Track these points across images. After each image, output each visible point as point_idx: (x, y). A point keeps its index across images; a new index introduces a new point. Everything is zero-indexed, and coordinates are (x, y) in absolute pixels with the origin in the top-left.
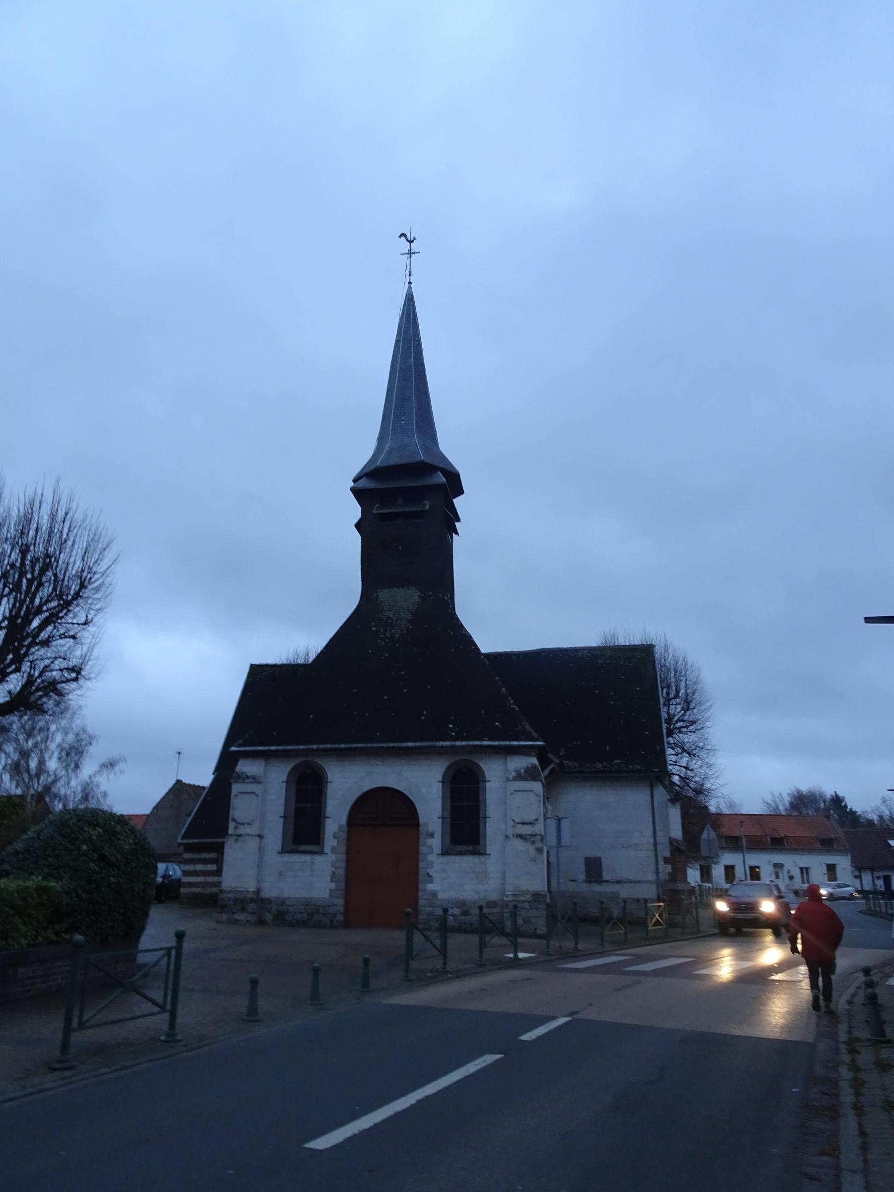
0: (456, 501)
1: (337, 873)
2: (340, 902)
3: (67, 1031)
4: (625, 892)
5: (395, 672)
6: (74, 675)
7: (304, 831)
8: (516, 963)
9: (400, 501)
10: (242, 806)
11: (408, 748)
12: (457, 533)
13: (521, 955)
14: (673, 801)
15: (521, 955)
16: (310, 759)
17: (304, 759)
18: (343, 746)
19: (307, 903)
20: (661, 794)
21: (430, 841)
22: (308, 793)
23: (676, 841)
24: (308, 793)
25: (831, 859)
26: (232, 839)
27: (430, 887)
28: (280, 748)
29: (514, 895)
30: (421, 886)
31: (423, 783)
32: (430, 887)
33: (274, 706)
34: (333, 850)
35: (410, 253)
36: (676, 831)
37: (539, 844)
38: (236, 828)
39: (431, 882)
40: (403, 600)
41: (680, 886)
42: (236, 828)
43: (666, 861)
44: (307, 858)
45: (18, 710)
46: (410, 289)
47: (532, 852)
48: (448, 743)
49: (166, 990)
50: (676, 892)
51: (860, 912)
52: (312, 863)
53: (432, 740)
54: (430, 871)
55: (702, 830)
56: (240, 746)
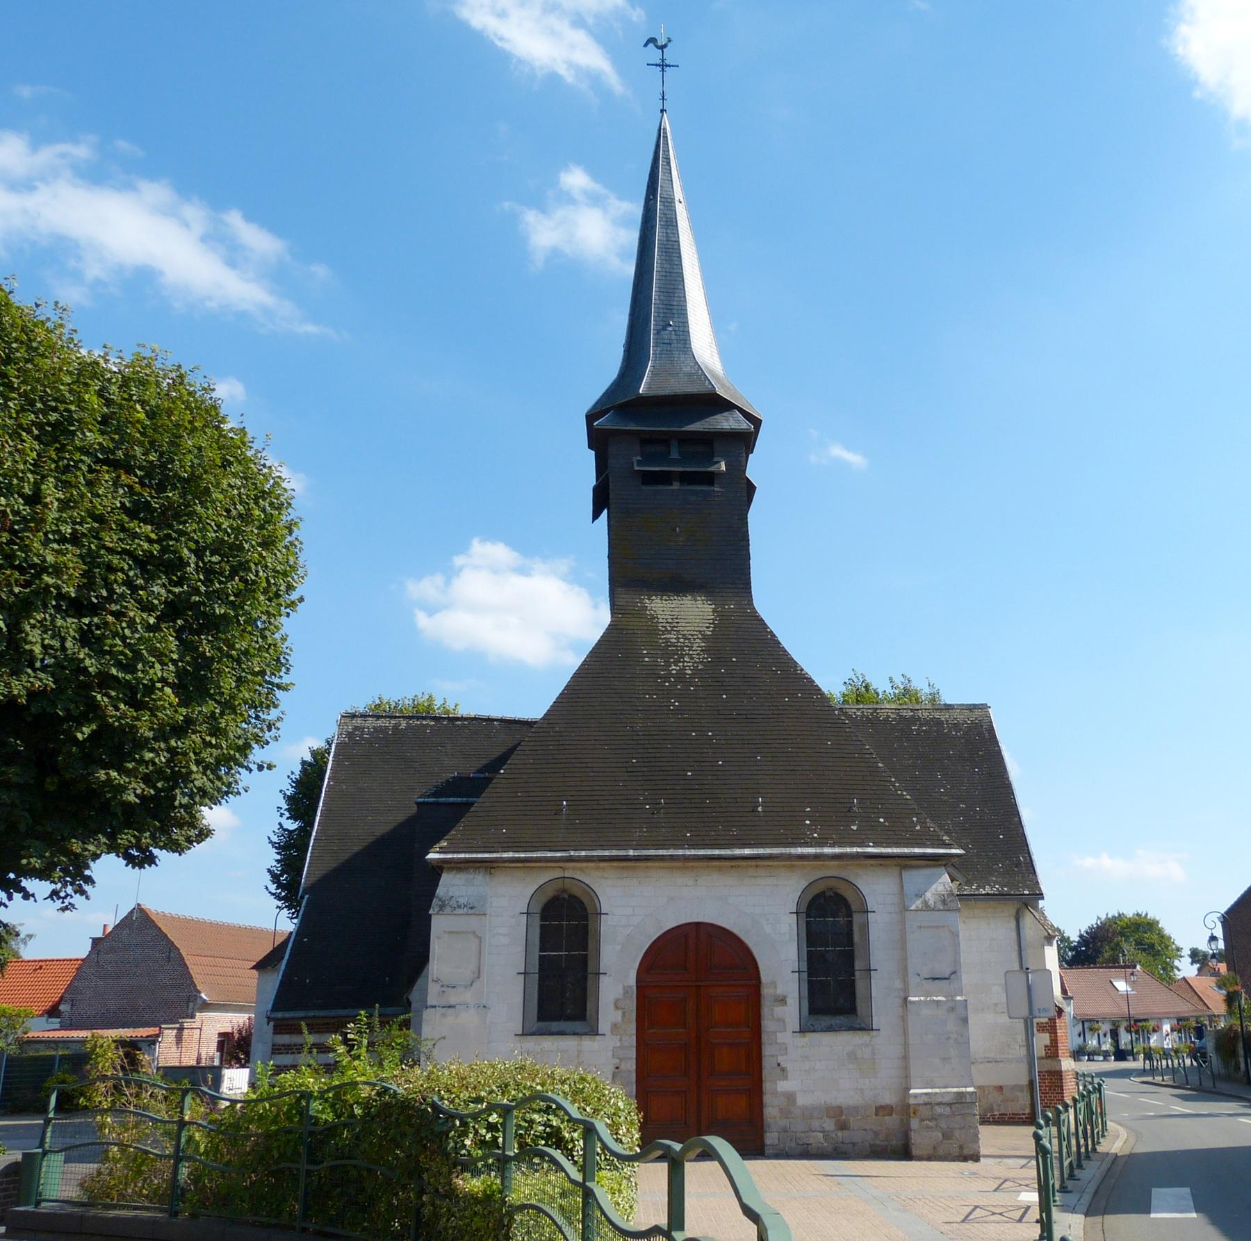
1: (623, 1067)
7: (560, 995)
9: (675, 455)
17: (558, 874)
21: (779, 1010)
22: (565, 929)
24: (565, 929)
27: (783, 1086)
30: (767, 1086)
32: (783, 1086)
34: (615, 1027)
39: (786, 1078)
40: (688, 614)
44: (568, 1043)
52: (579, 1052)
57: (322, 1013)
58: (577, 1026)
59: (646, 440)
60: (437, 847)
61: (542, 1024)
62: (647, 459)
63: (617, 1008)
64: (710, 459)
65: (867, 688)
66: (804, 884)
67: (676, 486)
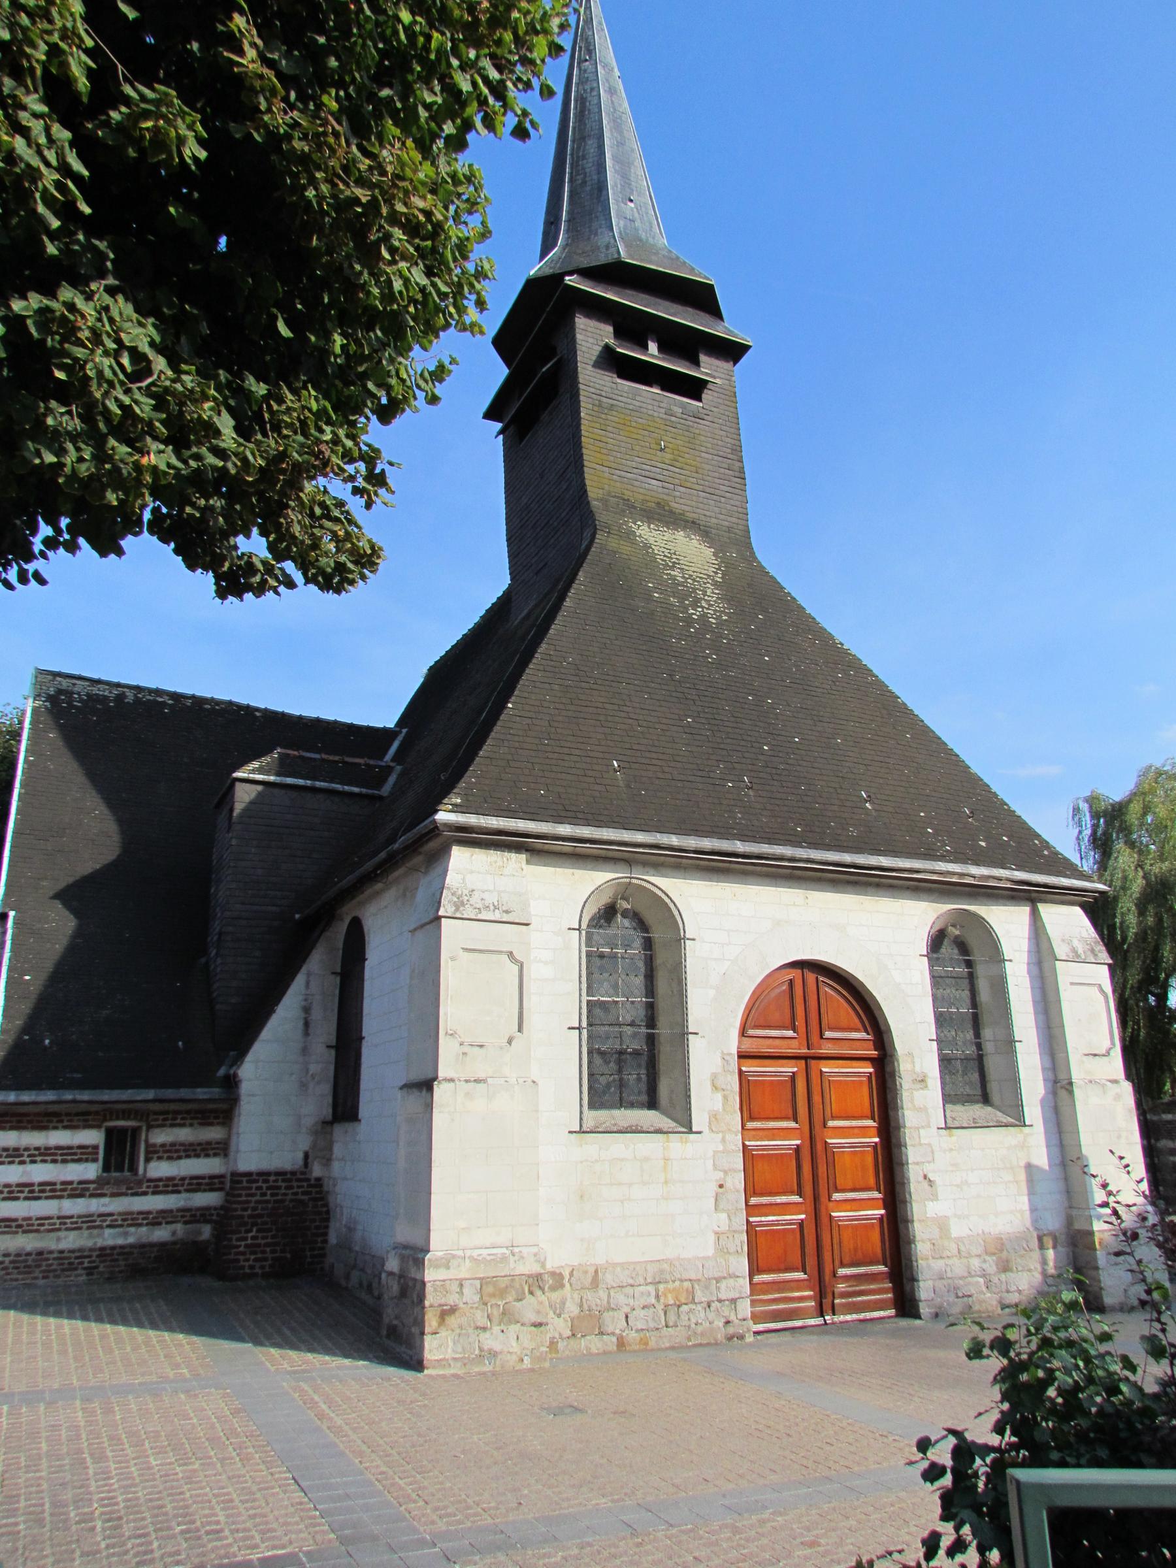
1: (729, 1184)
7: (633, 1067)
22: (637, 954)
24: (637, 954)
34: (714, 1117)
39: (935, 1197)
57: (85, 1096)
60: (256, 764)
61: (603, 1115)
63: (715, 1087)
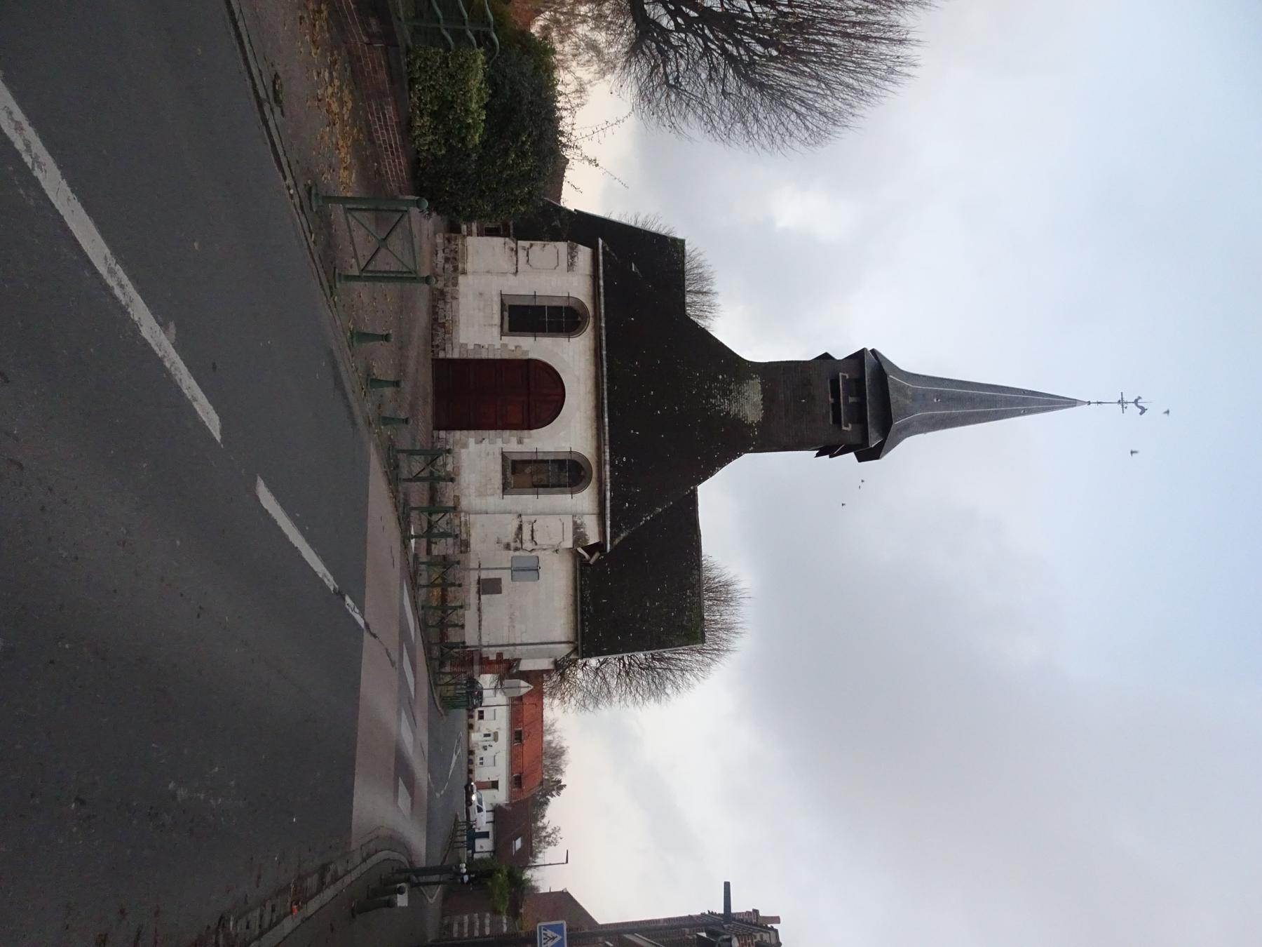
0: (852, 454)
2: (456, 356)
3: (345, 200)
4: (470, 617)
5: (679, 390)
6: (671, 82)
7: (524, 317)
8: (405, 545)
9: (851, 400)
10: (549, 253)
11: (603, 418)
12: (818, 455)
13: (413, 541)
14: (556, 662)
15: (413, 541)
16: (591, 319)
18: (604, 353)
19: (454, 322)
20: (564, 650)
21: (514, 440)
22: (557, 319)
23: (518, 665)
24: (557, 319)
25: (503, 785)
26: (513, 245)
27: (472, 441)
28: (602, 290)
29: (466, 524)
30: (472, 432)
31: (572, 431)
32: (472, 441)
33: (644, 275)
34: (505, 345)
35: (1121, 402)
36: (526, 665)
37: (513, 545)
38: (524, 248)
40: (750, 404)
41: (476, 668)
42: (524, 248)
43: (500, 655)
44: (497, 320)
45: (637, 28)
46: (1083, 403)
47: (505, 541)
48: (608, 458)
49: (427, 884)
50: (471, 663)
51: (456, 816)
53: (610, 441)
54: (486, 441)
55: (531, 688)
56: (604, 248)
58: (506, 326)
59: (860, 381)
62: (846, 382)
64: (850, 420)
65: (673, 125)
66: (582, 298)
67: (831, 400)
